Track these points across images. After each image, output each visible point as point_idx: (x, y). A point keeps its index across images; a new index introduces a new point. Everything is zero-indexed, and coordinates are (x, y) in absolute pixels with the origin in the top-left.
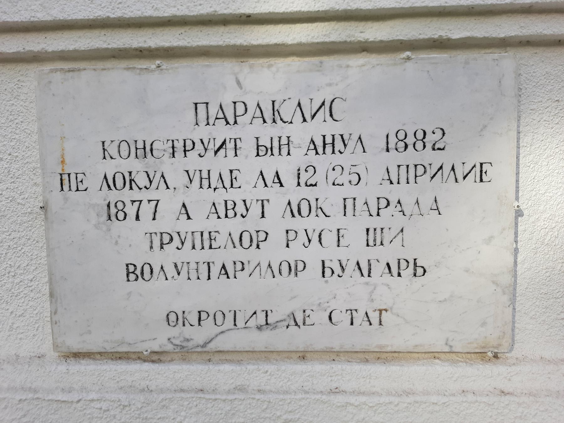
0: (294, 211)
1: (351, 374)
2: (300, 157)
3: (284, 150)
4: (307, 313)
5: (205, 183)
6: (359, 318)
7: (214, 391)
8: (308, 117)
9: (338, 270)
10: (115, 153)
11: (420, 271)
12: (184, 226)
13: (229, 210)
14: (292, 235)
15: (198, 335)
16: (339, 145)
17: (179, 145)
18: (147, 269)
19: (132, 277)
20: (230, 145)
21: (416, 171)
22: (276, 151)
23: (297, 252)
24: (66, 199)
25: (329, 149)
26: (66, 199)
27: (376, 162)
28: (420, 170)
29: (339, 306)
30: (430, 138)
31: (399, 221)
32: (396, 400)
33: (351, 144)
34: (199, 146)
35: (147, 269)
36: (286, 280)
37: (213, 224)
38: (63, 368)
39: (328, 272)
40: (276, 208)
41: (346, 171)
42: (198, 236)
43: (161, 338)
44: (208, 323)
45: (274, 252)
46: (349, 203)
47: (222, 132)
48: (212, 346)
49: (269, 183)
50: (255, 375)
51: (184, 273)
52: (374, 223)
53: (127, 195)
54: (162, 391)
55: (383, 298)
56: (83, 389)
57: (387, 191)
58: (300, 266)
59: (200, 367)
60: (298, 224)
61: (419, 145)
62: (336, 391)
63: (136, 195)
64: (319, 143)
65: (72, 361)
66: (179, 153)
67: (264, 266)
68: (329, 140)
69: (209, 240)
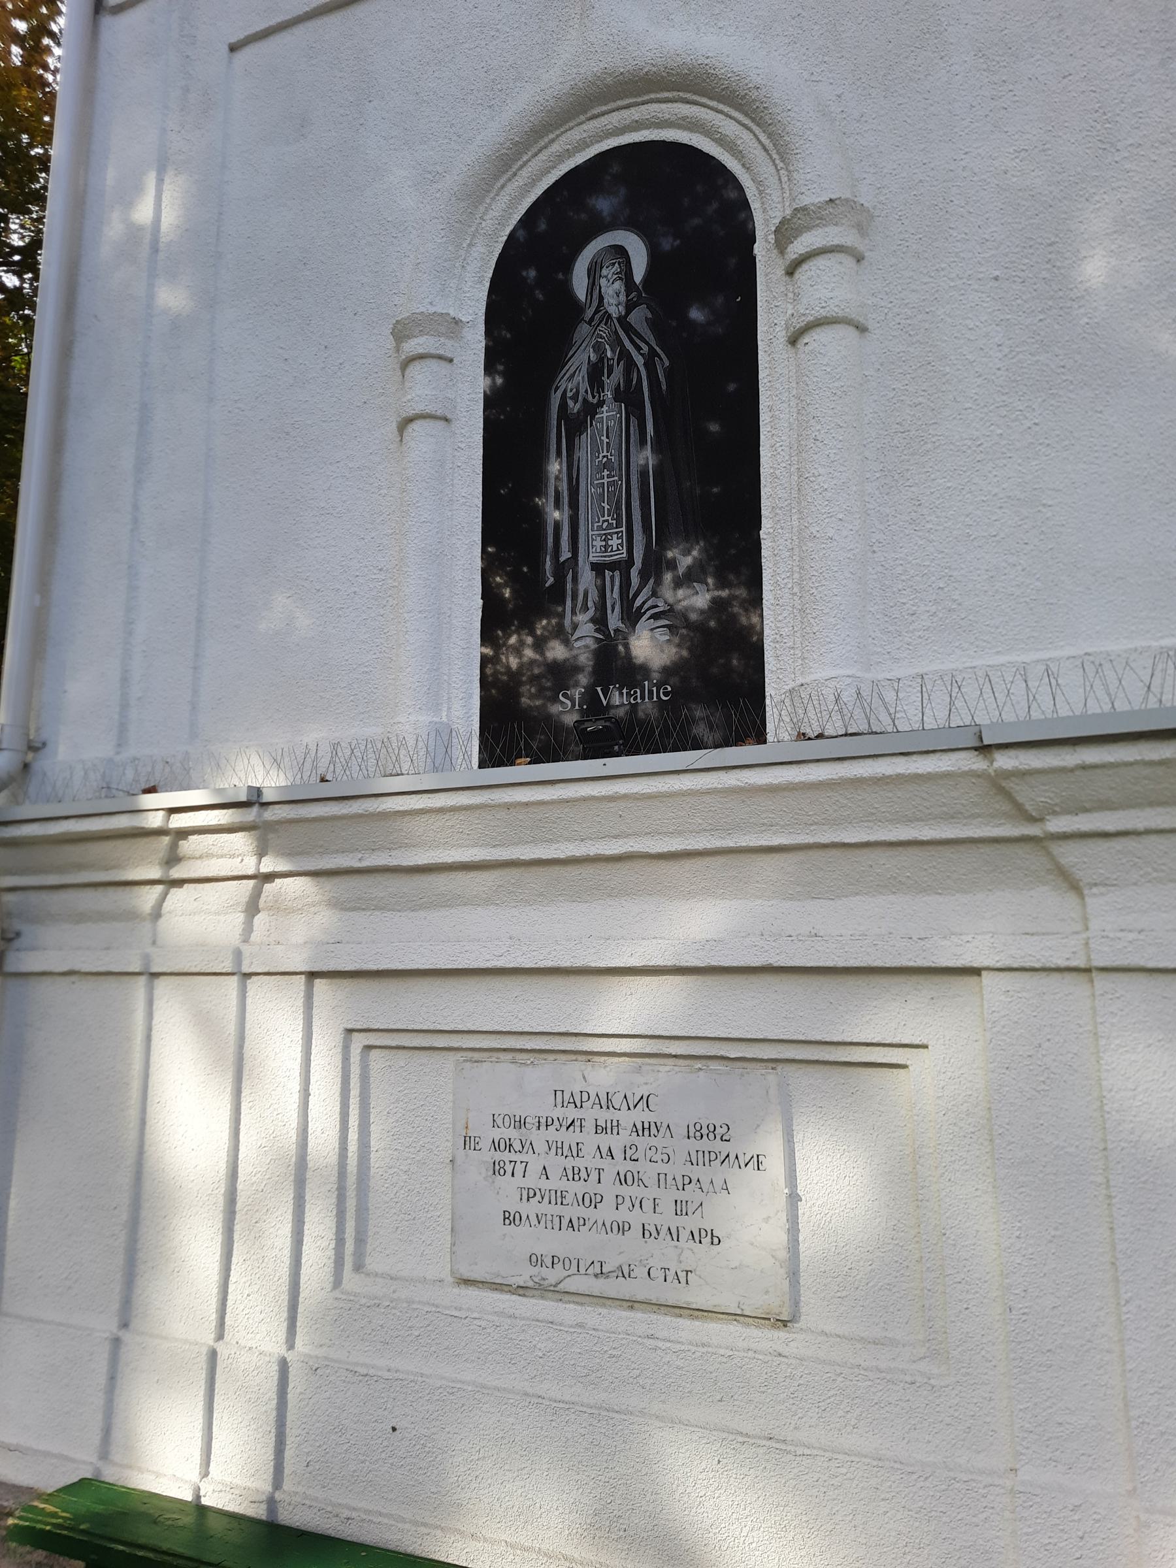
0: (622, 1180)
1: (664, 1323)
2: (625, 1137)
3: (615, 1131)
4: (632, 1267)
5: (560, 1151)
6: (671, 1276)
7: (561, 1325)
8: (632, 1107)
9: (654, 1234)
10: (501, 1124)
11: (716, 1240)
12: (544, 1185)
13: (574, 1174)
14: (620, 1200)
15: (552, 1276)
16: (653, 1130)
17: (543, 1121)
18: (517, 1216)
19: (507, 1221)
20: (577, 1124)
21: (709, 1157)
22: (609, 1130)
23: (623, 1215)
24: (467, 1156)
25: (646, 1132)
26: (467, 1156)
27: (682, 1146)
28: (713, 1156)
29: (656, 1264)
30: (719, 1131)
31: (698, 1196)
32: (693, 1349)
33: (662, 1130)
34: (556, 1122)
35: (517, 1216)
36: (615, 1237)
37: (563, 1185)
38: (456, 1290)
39: (647, 1234)
40: (608, 1176)
41: (659, 1151)
42: (553, 1193)
43: (524, 1275)
44: (558, 1267)
45: (606, 1213)
46: (662, 1177)
47: (572, 1113)
48: (561, 1287)
49: (604, 1155)
50: (591, 1315)
51: (543, 1222)
52: (681, 1195)
53: (507, 1156)
54: (523, 1319)
55: (689, 1262)
56: (469, 1309)
57: (689, 1170)
58: (626, 1228)
59: (552, 1303)
60: (625, 1190)
61: (711, 1136)
62: (651, 1337)
63: (513, 1157)
64: (640, 1127)
65: (463, 1286)
66: (543, 1127)
67: (600, 1223)
68: (646, 1126)
69: (560, 1197)
